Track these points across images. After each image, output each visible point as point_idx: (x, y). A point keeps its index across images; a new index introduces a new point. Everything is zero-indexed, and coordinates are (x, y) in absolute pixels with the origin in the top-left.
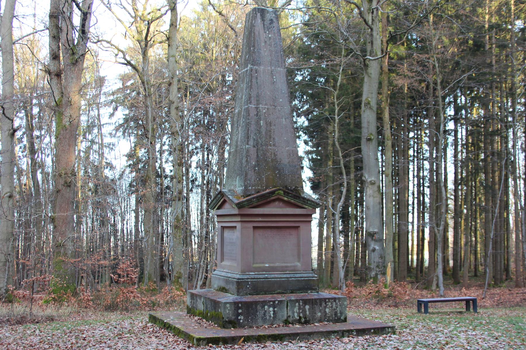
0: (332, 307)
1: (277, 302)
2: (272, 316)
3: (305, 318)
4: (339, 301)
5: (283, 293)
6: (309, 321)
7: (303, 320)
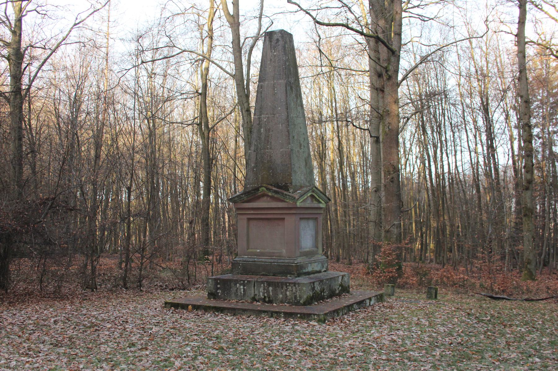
0: (292, 291)
1: (246, 282)
2: (242, 292)
3: (269, 298)
4: (299, 286)
5: (267, 275)
6: (272, 300)
7: (267, 299)
